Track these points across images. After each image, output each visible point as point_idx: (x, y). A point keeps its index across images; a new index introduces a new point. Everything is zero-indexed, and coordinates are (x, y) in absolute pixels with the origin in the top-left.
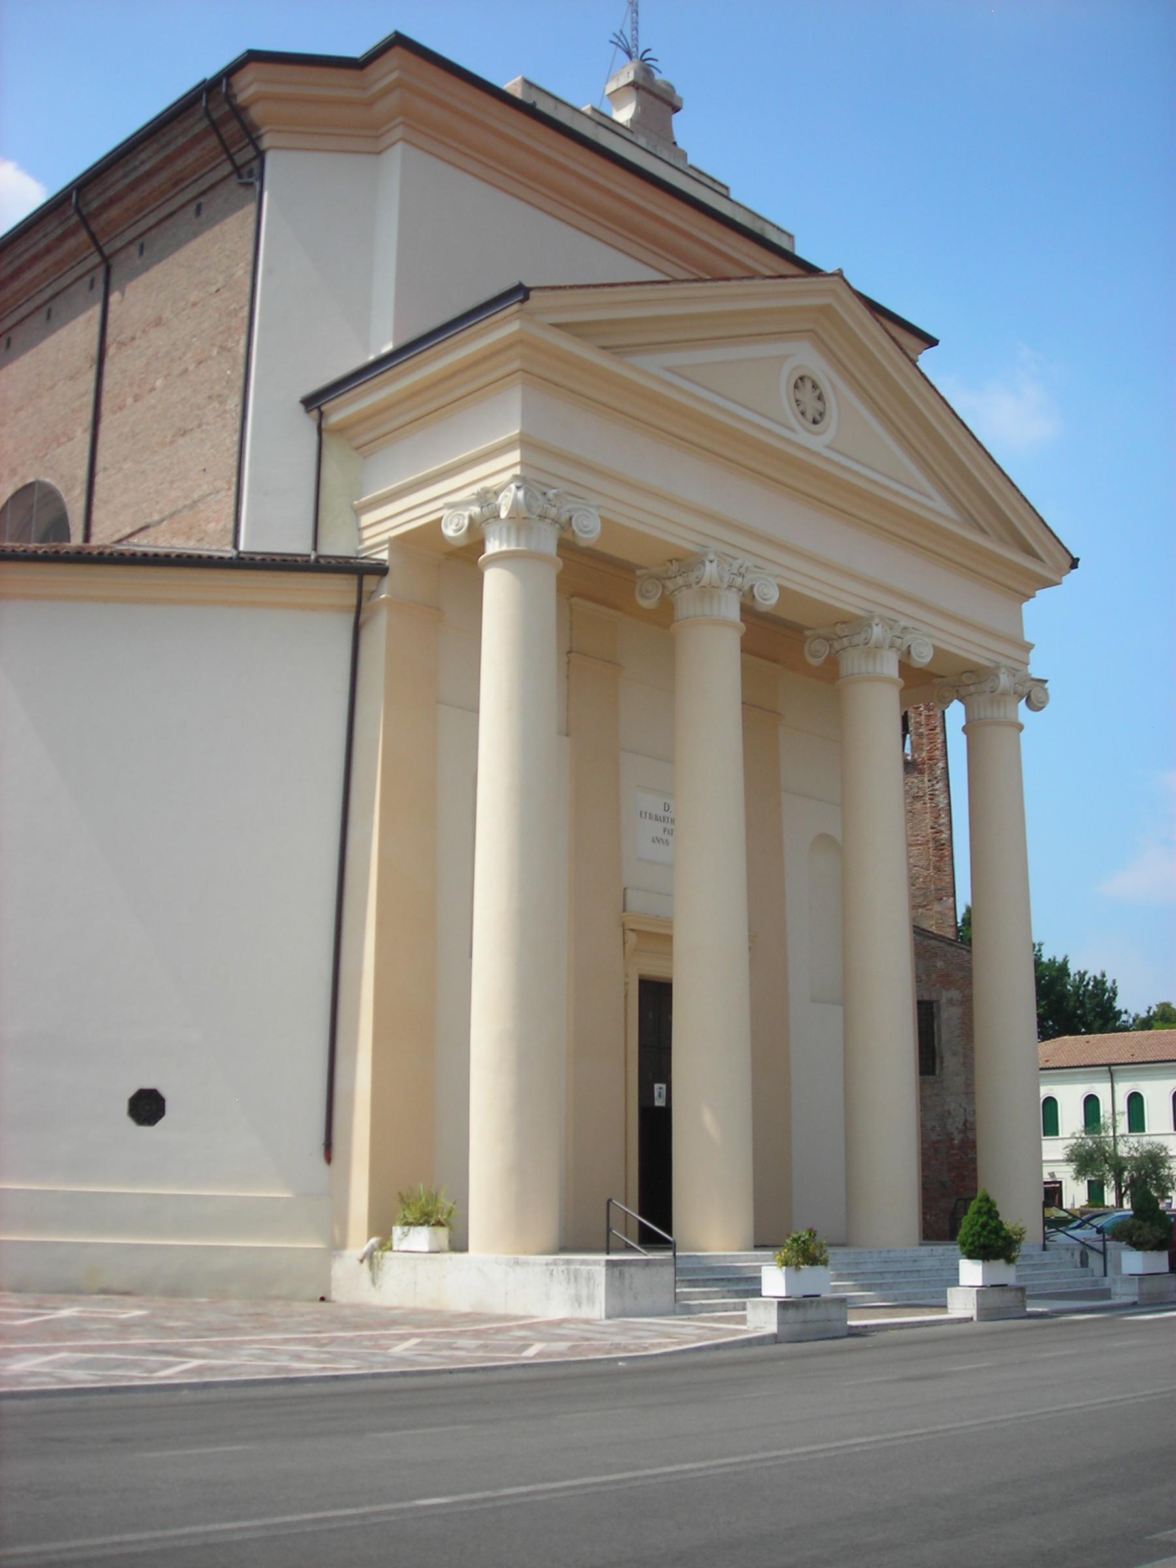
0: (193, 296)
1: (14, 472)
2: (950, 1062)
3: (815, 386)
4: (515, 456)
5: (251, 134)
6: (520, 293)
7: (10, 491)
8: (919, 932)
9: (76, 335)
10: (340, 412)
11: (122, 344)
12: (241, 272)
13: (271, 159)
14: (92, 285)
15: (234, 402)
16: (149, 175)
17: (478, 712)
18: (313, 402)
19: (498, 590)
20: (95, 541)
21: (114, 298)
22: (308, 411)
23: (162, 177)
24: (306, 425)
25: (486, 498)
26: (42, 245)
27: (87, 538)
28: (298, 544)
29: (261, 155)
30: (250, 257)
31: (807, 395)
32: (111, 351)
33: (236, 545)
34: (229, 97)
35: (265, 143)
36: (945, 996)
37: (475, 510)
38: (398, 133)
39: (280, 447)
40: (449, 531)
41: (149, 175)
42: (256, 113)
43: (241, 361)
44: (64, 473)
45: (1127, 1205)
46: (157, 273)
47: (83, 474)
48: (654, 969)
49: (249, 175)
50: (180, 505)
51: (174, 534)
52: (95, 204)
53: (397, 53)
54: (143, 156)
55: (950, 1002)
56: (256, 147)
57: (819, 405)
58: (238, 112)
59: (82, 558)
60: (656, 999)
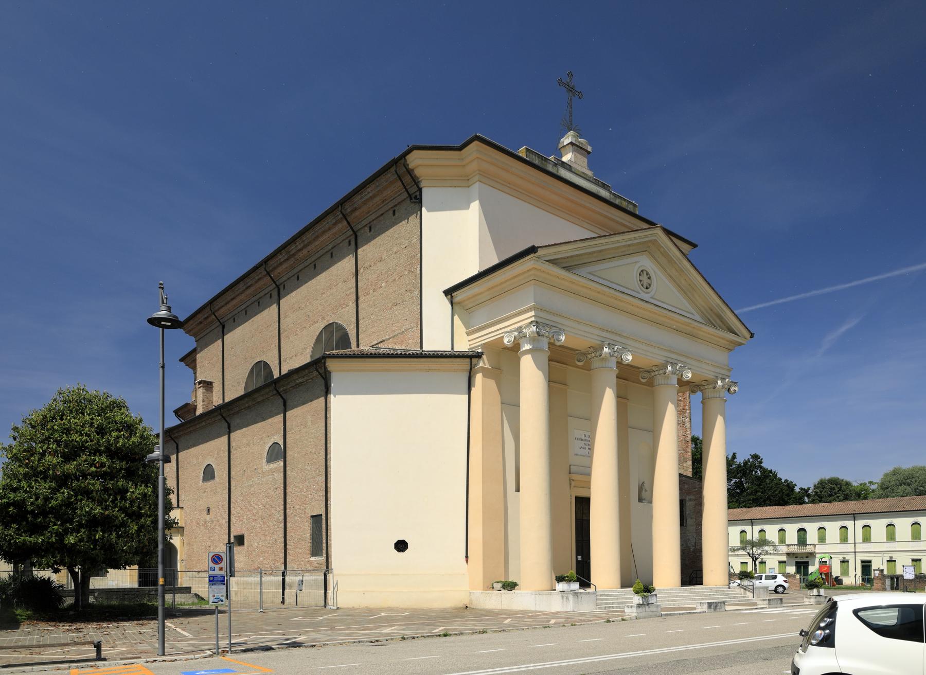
0: (395, 249)
1: (323, 318)
2: (690, 521)
3: (647, 274)
4: (532, 313)
5: (416, 182)
6: (532, 250)
7: (323, 326)
8: (680, 475)
9: (346, 265)
10: (459, 296)
11: (366, 268)
12: (415, 239)
13: (424, 191)
14: (350, 244)
15: (417, 292)
16: (371, 198)
17: (518, 406)
18: (449, 292)
19: (527, 364)
20: (362, 348)
21: (360, 251)
22: (446, 295)
23: (377, 199)
24: (446, 302)
25: (519, 330)
26: (327, 226)
27: (358, 346)
28: (445, 347)
29: (420, 190)
30: (419, 233)
31: (644, 278)
32: (361, 271)
33: (421, 347)
34: (406, 166)
35: (422, 185)
36: (688, 498)
37: (516, 333)
38: (477, 178)
39: (436, 309)
40: (506, 341)
41: (371, 198)
42: (418, 172)
43: (419, 276)
44: (346, 319)
45: (566, 140)
46: (378, 240)
47: (354, 320)
48: (582, 493)
49: (416, 200)
50: (397, 332)
51: (395, 343)
52: (349, 210)
53: (476, 143)
54: (369, 190)
55: (690, 500)
56: (418, 187)
57: (649, 281)
58: (410, 172)
59: (422, 356)
60: (583, 505)
